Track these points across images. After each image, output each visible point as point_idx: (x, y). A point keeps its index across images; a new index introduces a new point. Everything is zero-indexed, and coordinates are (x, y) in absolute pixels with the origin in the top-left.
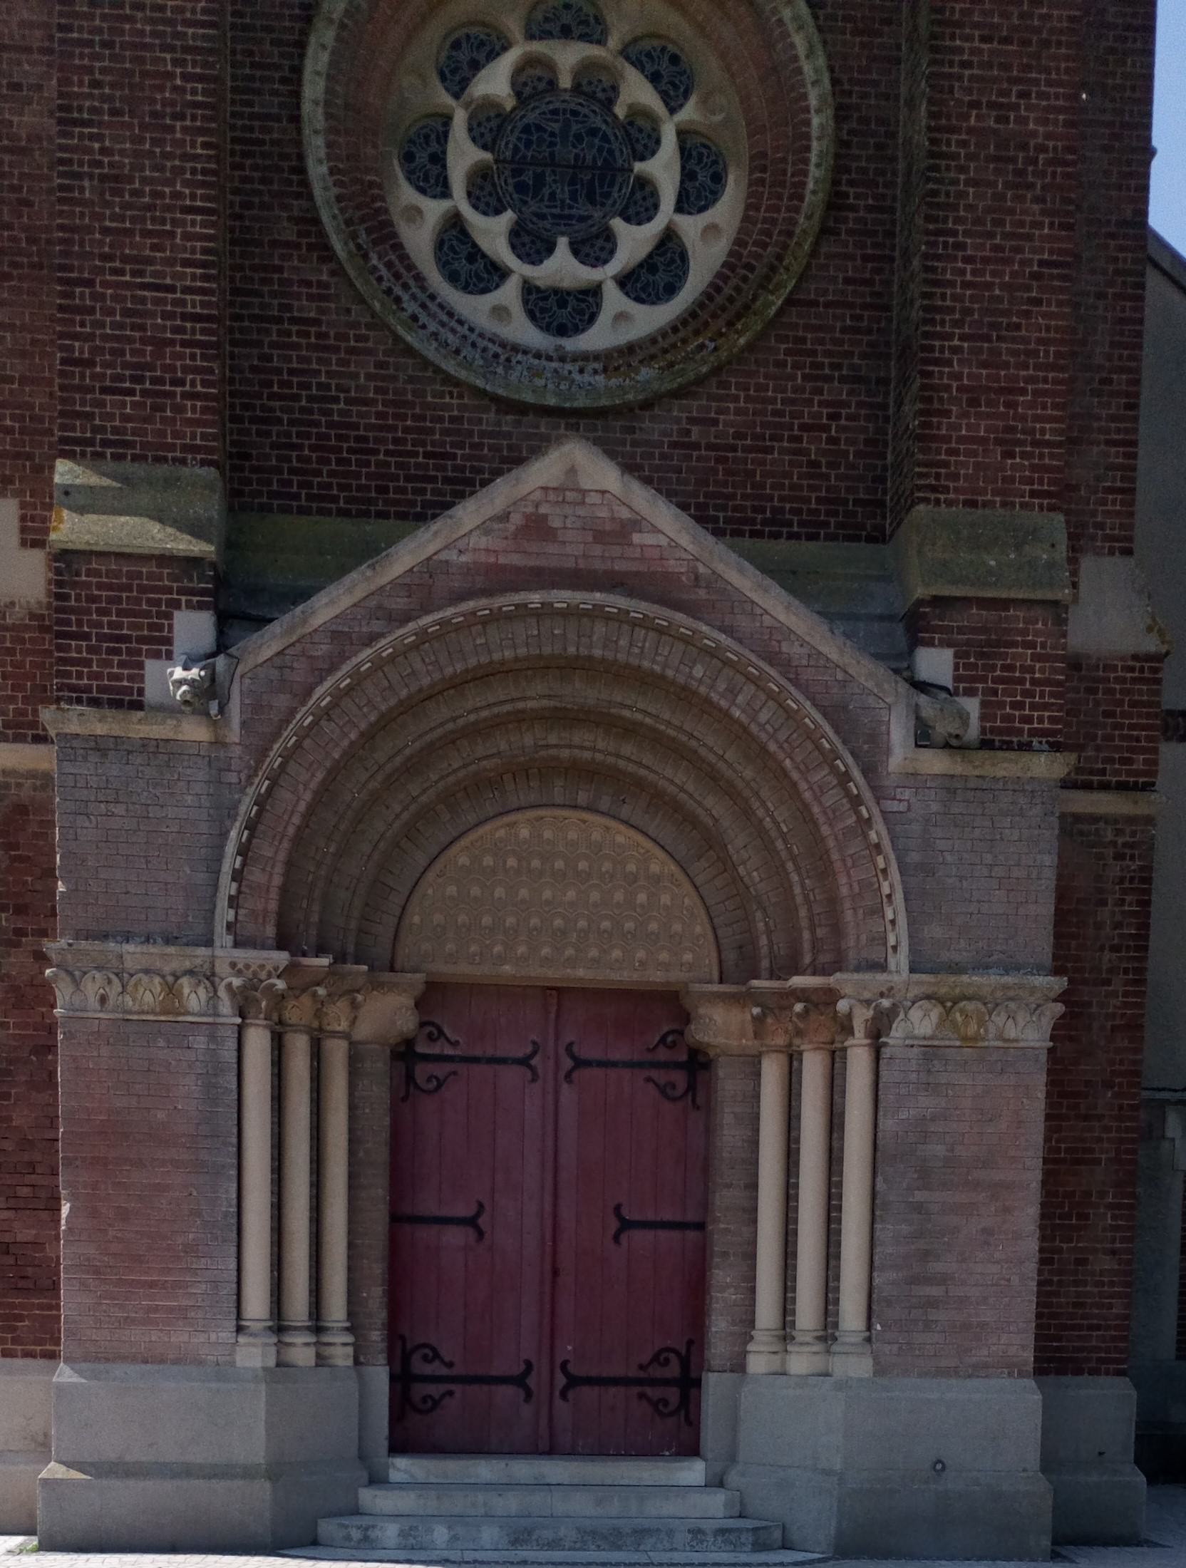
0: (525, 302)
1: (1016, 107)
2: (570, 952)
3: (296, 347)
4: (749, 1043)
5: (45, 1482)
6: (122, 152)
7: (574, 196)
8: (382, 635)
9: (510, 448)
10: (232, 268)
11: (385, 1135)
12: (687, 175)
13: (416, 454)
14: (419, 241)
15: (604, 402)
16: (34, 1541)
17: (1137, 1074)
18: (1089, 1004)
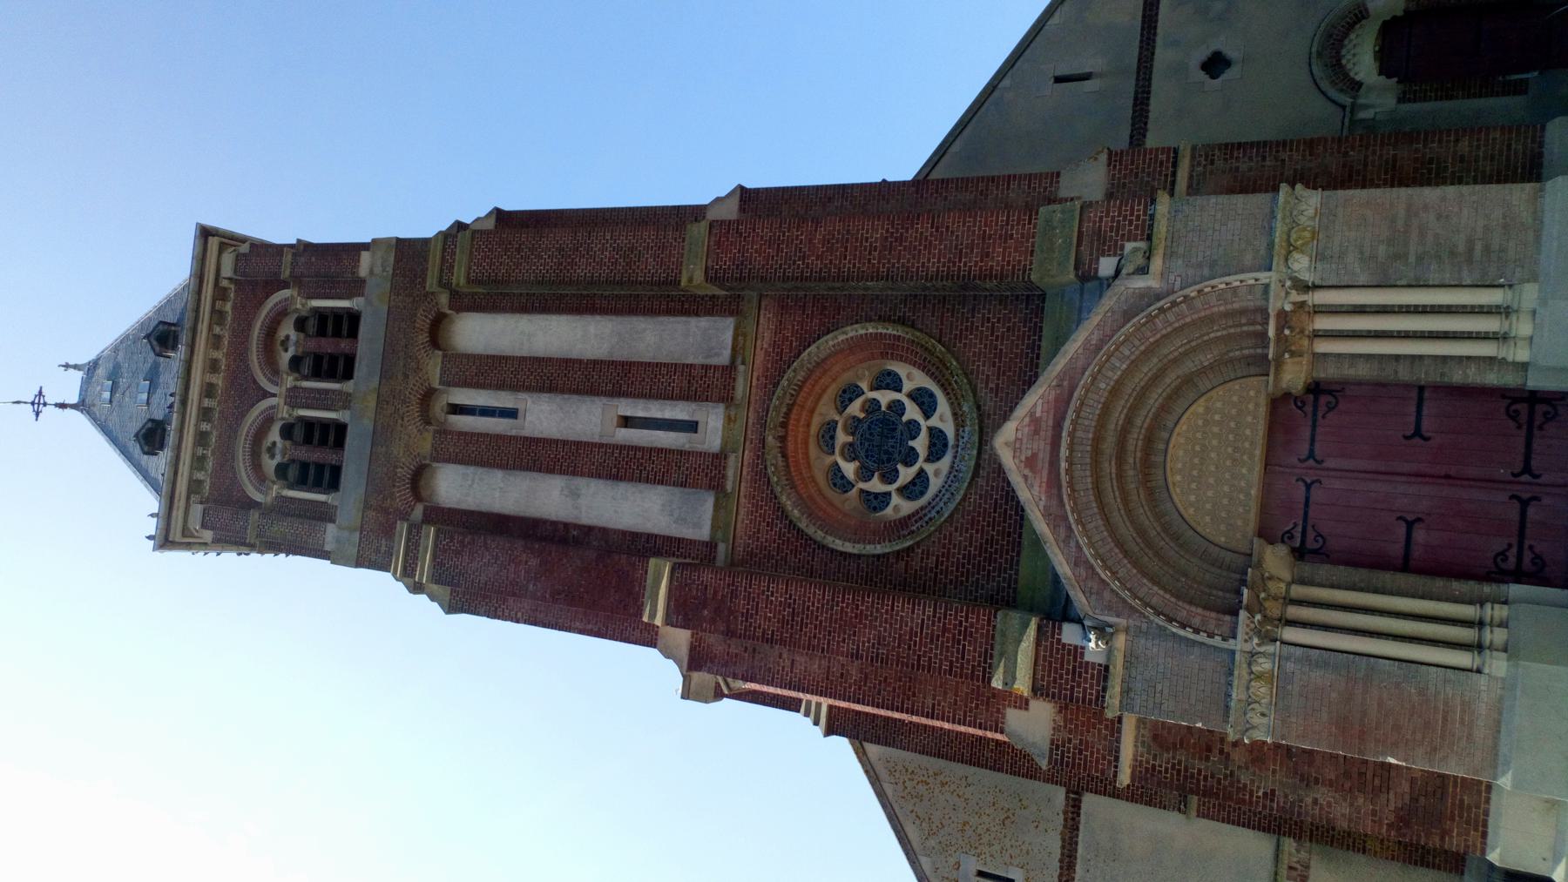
4: (1305, 360)
11: (1350, 569)
12: (887, 387)
14: (906, 507)
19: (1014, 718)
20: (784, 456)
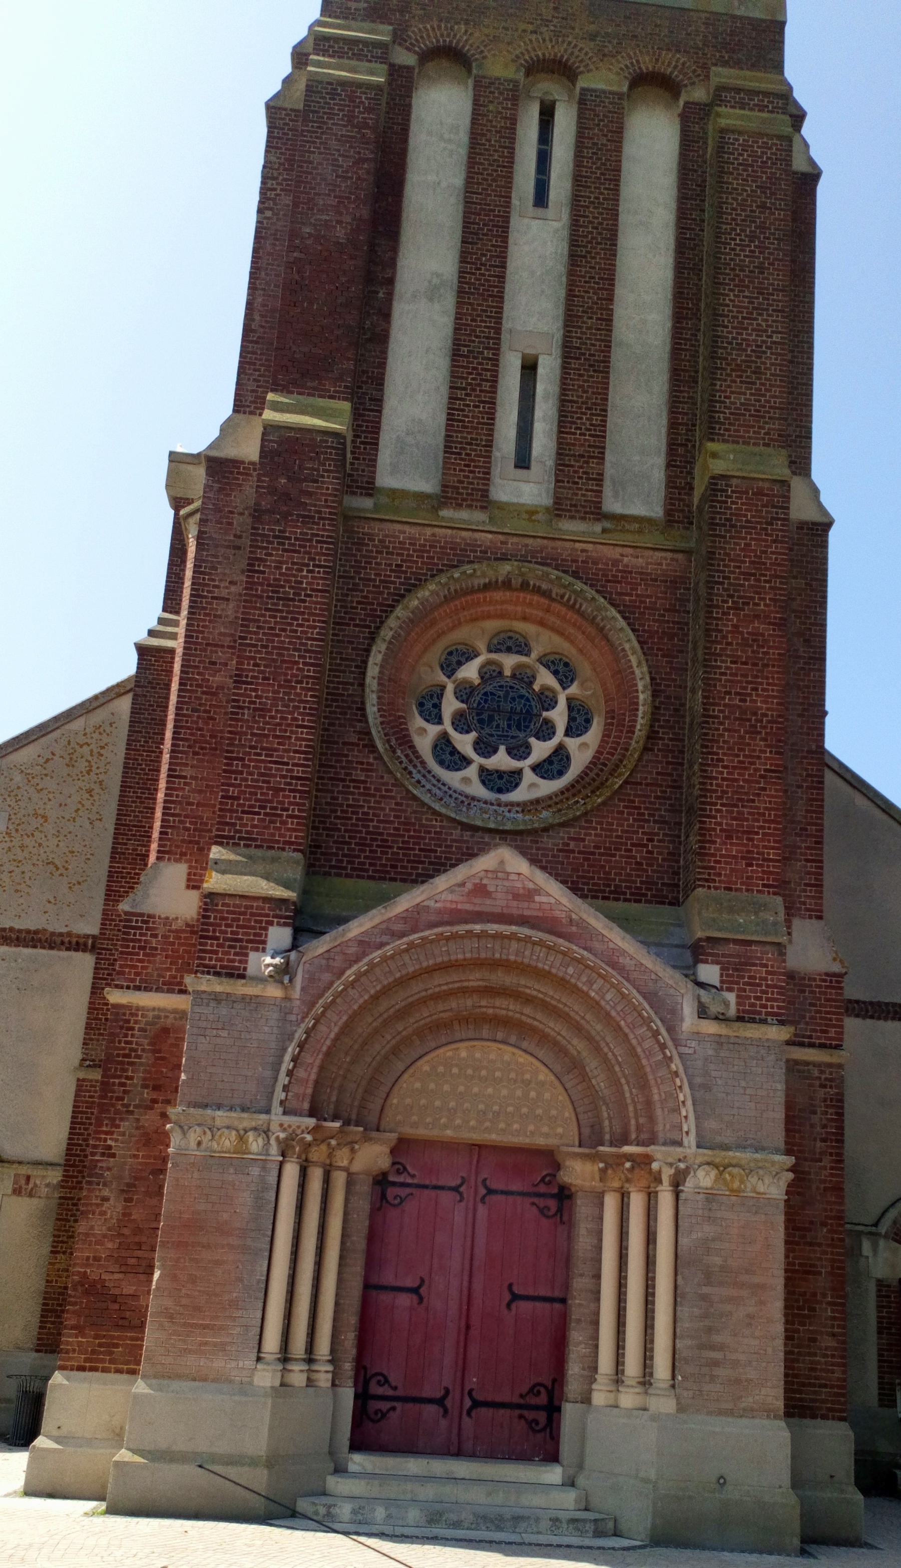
0: (480, 776)
1: (750, 695)
2: (487, 1124)
3: (353, 794)
4: (597, 1184)
5: (117, 1463)
6: (267, 698)
7: (509, 726)
8: (388, 944)
9: (468, 848)
10: (321, 754)
11: (365, 1232)
12: (571, 719)
13: (414, 849)
15: (522, 827)
16: (103, 1506)
17: (841, 1218)
18: (809, 1173)
19: (175, 873)
20: (486, 587)
